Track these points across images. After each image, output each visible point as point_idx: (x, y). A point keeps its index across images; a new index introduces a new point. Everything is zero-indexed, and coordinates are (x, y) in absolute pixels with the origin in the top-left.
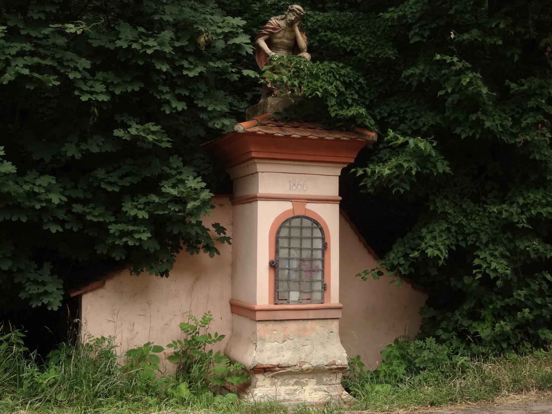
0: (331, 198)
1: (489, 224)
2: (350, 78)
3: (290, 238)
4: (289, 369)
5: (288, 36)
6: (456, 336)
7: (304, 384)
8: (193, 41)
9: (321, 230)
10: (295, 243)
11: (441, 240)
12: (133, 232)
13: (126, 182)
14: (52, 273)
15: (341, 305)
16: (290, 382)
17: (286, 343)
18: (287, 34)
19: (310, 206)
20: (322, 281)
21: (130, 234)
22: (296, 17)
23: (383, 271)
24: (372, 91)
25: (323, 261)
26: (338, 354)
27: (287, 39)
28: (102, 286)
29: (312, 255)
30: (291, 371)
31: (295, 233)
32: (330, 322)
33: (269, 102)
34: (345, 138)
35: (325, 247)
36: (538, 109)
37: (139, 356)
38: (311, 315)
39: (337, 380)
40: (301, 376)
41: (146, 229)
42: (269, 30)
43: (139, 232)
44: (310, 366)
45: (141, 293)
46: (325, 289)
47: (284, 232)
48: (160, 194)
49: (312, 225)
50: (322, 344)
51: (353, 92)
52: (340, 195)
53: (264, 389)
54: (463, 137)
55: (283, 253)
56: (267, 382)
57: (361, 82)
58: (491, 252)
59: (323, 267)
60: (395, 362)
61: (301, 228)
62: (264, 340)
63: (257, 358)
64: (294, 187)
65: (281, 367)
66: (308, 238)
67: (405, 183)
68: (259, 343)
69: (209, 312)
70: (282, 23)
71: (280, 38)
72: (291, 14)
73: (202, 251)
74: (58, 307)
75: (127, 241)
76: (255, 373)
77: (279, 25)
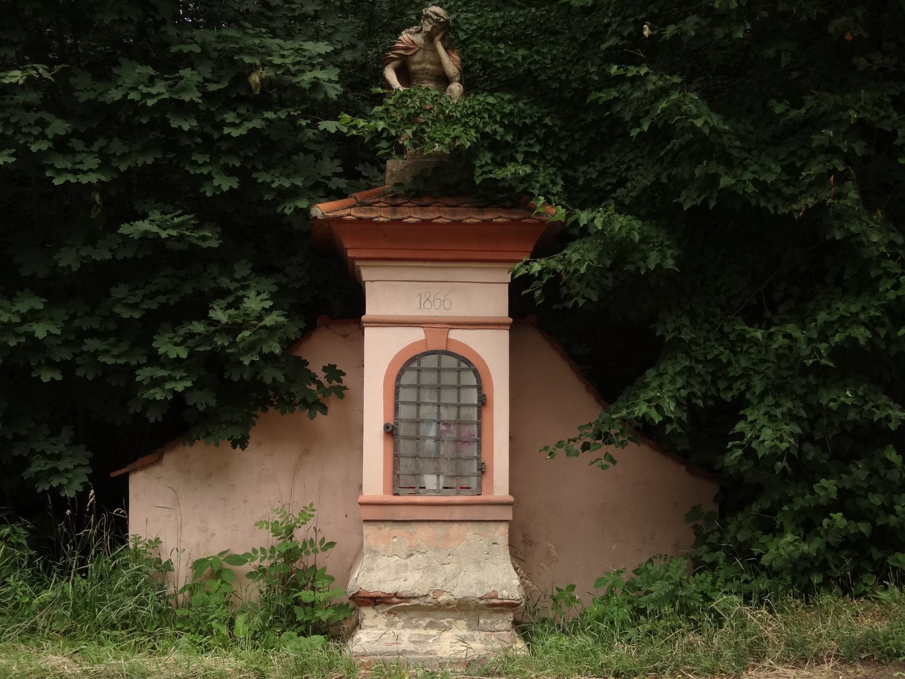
1: (774, 360)
2: (525, 118)
3: (418, 387)
5: (431, 58)
8: (241, 77)
9: (476, 372)
10: (427, 396)
11: (672, 388)
12: (164, 380)
14: (75, 441)
15: (511, 499)
16: (421, 622)
17: (413, 558)
19: (456, 335)
22: (434, 27)
24: (577, 136)
25: (479, 425)
26: (503, 579)
27: (431, 63)
28: (158, 460)
29: (458, 416)
30: (419, 605)
31: (428, 378)
32: (492, 526)
34: (499, 220)
35: (483, 402)
36: (831, 150)
37: (213, 571)
39: (503, 623)
40: (440, 614)
42: (398, 52)
45: (216, 473)
46: (483, 473)
47: (409, 378)
49: (459, 364)
50: (477, 562)
51: (531, 142)
52: (510, 315)
54: (685, 208)
57: (547, 124)
58: (768, 409)
59: (479, 435)
62: (375, 552)
64: (428, 305)
65: (402, 598)
66: (452, 387)
68: (367, 556)
69: (312, 505)
70: (419, 39)
71: (420, 63)
74: (77, 492)
76: (360, 606)
77: (413, 42)
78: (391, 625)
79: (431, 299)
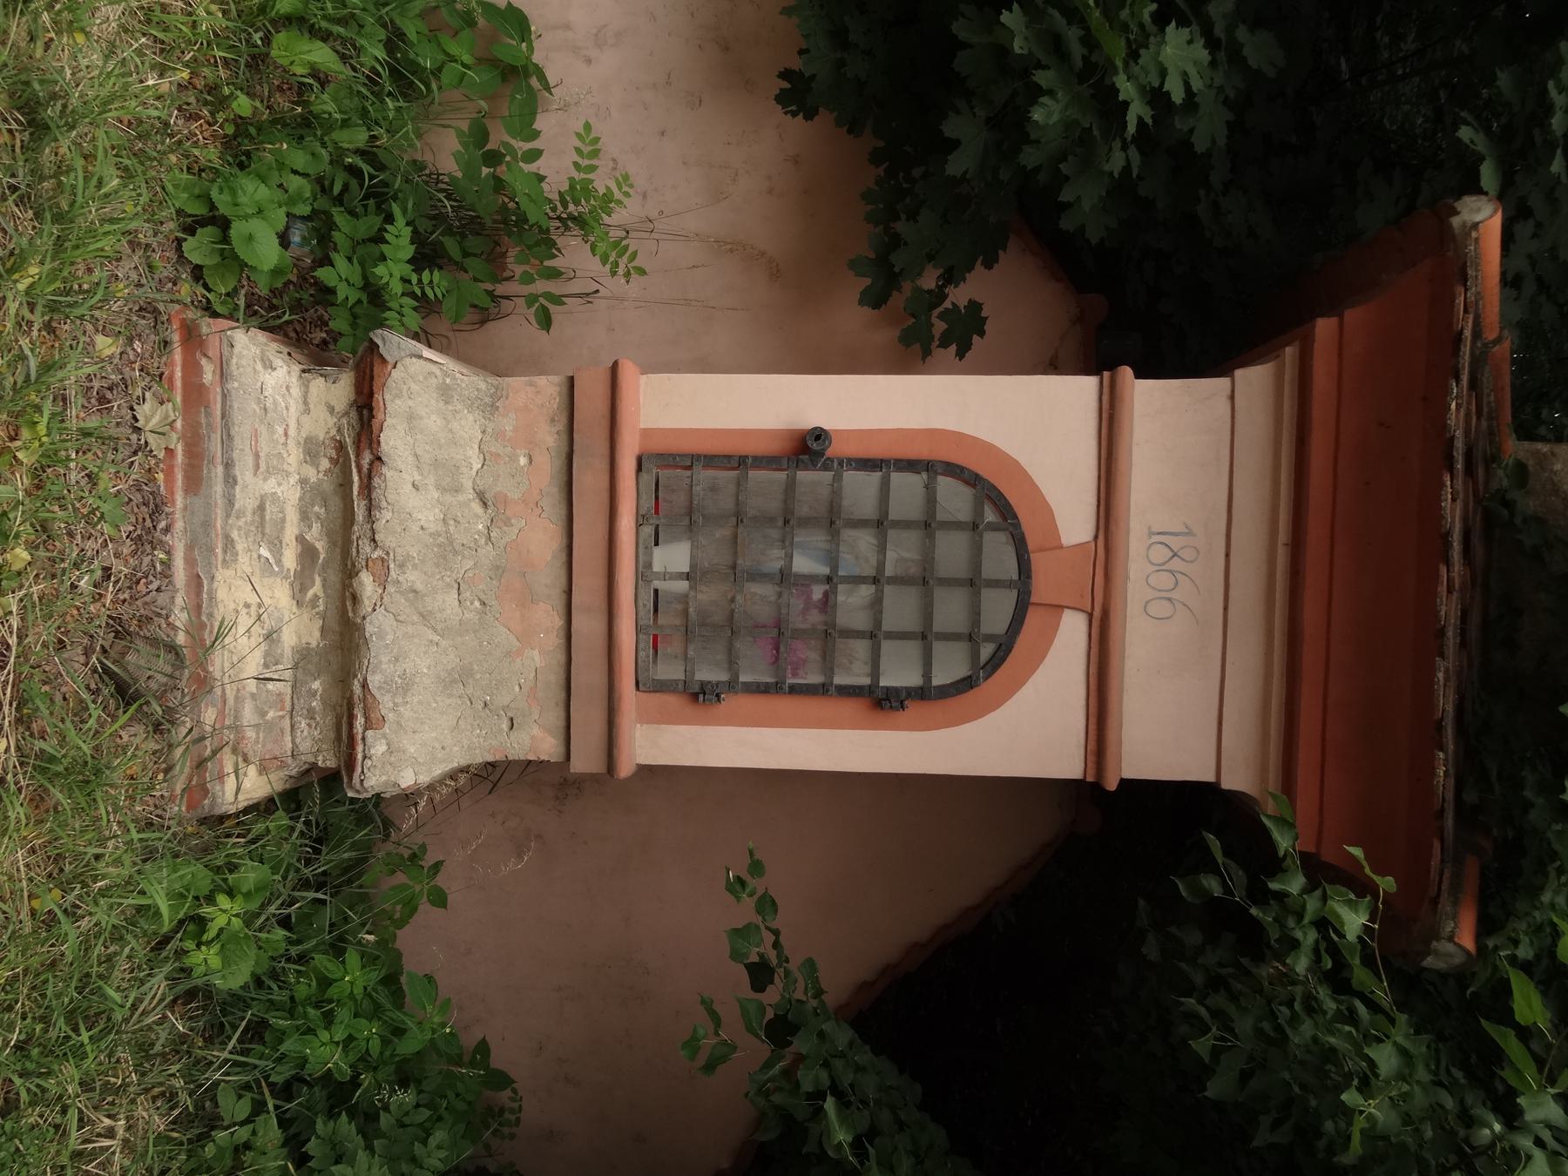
0: (1111, 736)
7: (303, 589)
9: (966, 684)
15: (625, 769)
16: (316, 527)
17: (477, 507)
19: (1073, 631)
20: (732, 686)
23: (772, 995)
25: (820, 690)
31: (951, 552)
32: (555, 717)
35: (884, 703)
38: (588, 626)
40: (334, 577)
44: (367, 605)
47: (954, 499)
49: (990, 638)
52: (1125, 783)
53: (295, 409)
56: (322, 425)
59: (795, 690)
60: (370, 1032)
61: (971, 583)
62: (491, 408)
64: (1159, 554)
65: (370, 477)
67: (1245, 1076)
78: (311, 450)
79: (1176, 564)
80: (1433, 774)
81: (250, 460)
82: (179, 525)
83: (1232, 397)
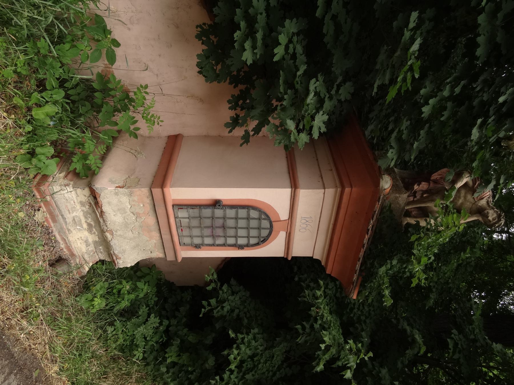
4: (101, 220)
6: (163, 340)
13: (328, 28)
15: (180, 260)
18: (468, 205)
19: (282, 236)
21: (251, 33)
25: (224, 245)
27: (462, 204)
31: (254, 223)
33: (402, 196)
38: (166, 237)
40: (98, 228)
41: (258, 57)
43: (254, 47)
48: (309, 75)
49: (262, 237)
52: (293, 257)
55: (231, 213)
59: (218, 245)
62: (131, 195)
63: (106, 191)
68: (126, 190)
70: (483, 202)
71: (465, 197)
72: (495, 215)
73: (232, 113)
75: (240, 30)
77: (483, 198)
78: (82, 204)
79: (307, 223)
80: (353, 277)
81: (67, 212)
82: (54, 229)
83: (324, 194)
